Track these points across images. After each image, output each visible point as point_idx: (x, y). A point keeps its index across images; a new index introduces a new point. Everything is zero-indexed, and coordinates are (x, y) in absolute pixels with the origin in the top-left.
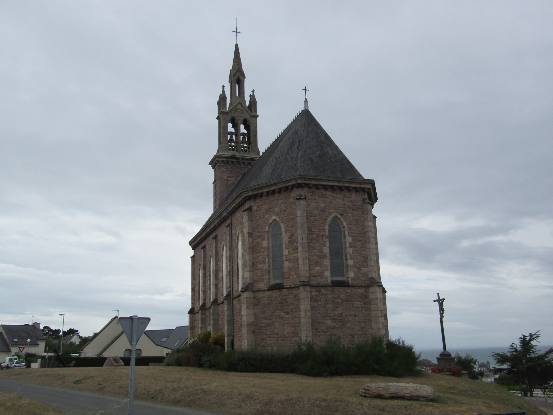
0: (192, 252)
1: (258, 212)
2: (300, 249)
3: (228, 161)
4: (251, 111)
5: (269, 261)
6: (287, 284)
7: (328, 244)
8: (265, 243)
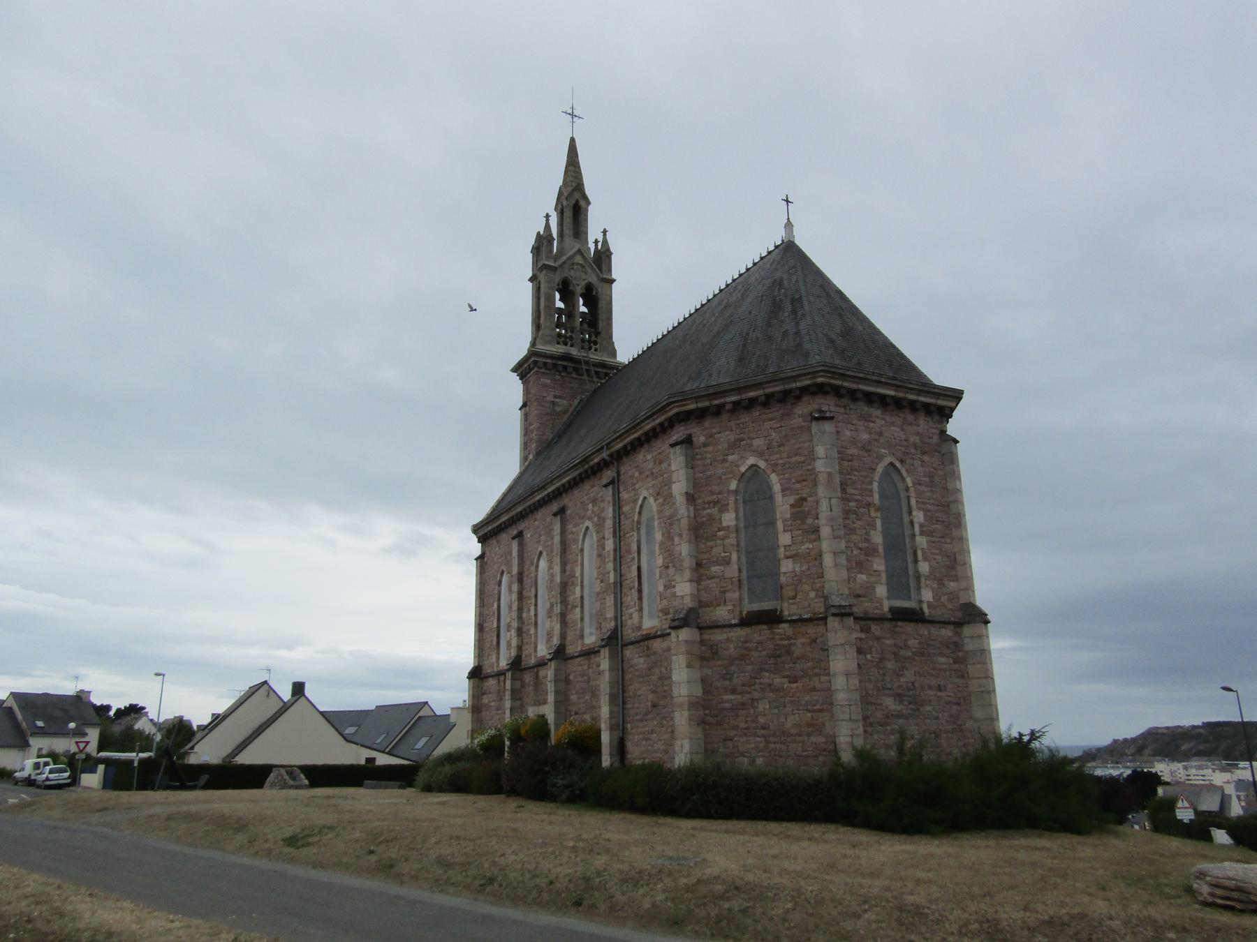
0: (477, 548)
1: (710, 448)
2: (825, 531)
3: (555, 365)
4: (600, 269)
5: (739, 559)
6: (788, 610)
7: (879, 523)
8: (729, 519)
